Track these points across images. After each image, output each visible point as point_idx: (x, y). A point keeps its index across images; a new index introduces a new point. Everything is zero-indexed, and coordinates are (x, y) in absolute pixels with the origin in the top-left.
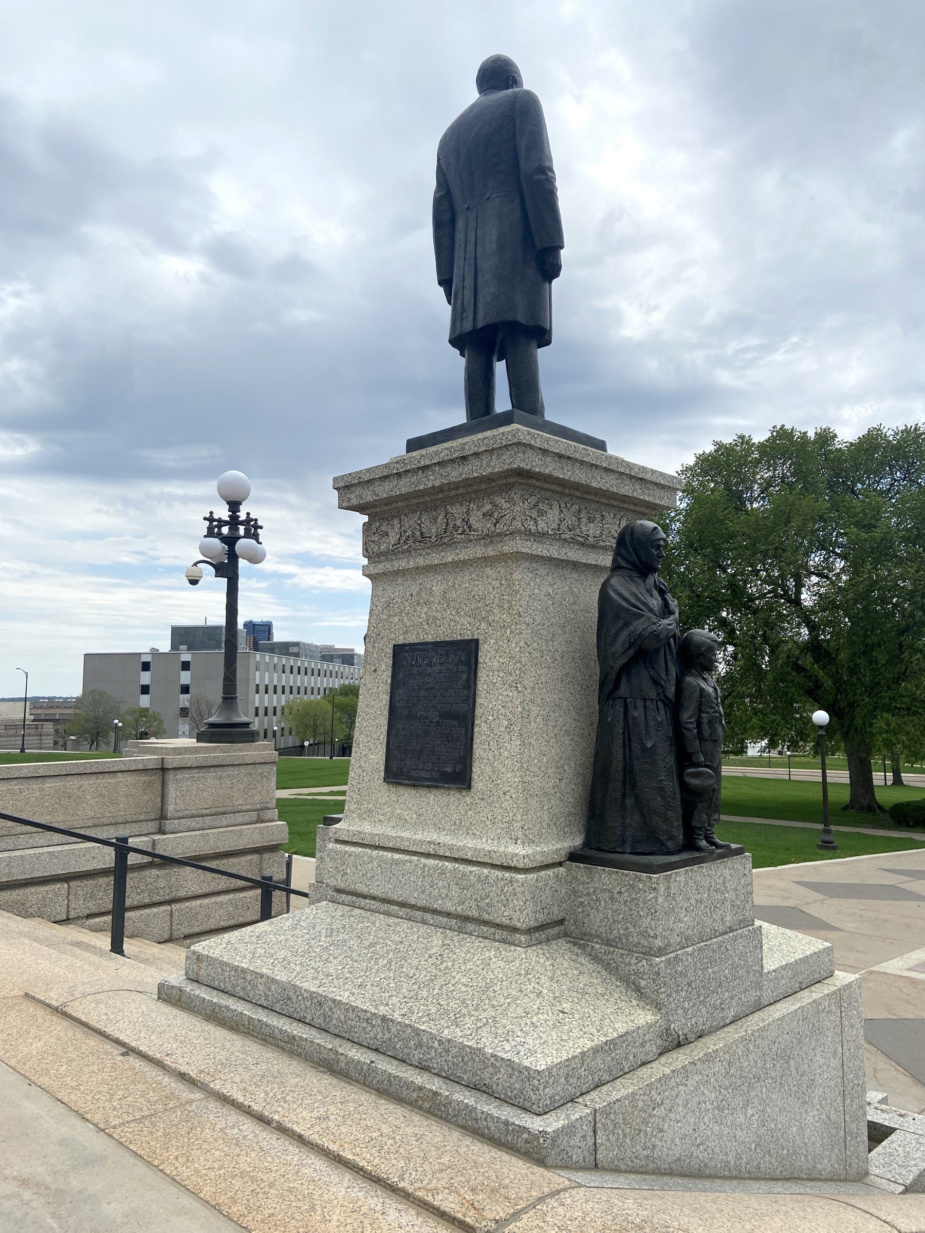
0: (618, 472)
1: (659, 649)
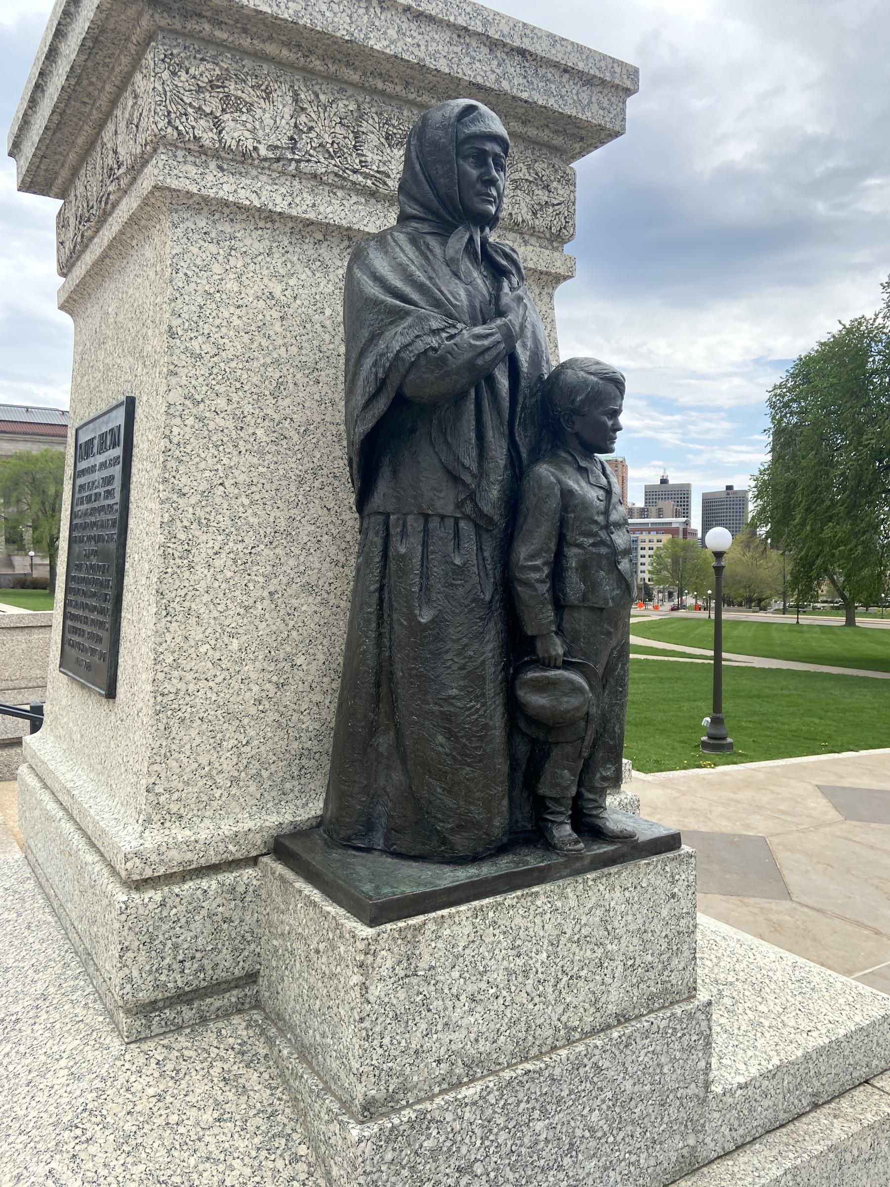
0: (449, 25)
1: (464, 395)
